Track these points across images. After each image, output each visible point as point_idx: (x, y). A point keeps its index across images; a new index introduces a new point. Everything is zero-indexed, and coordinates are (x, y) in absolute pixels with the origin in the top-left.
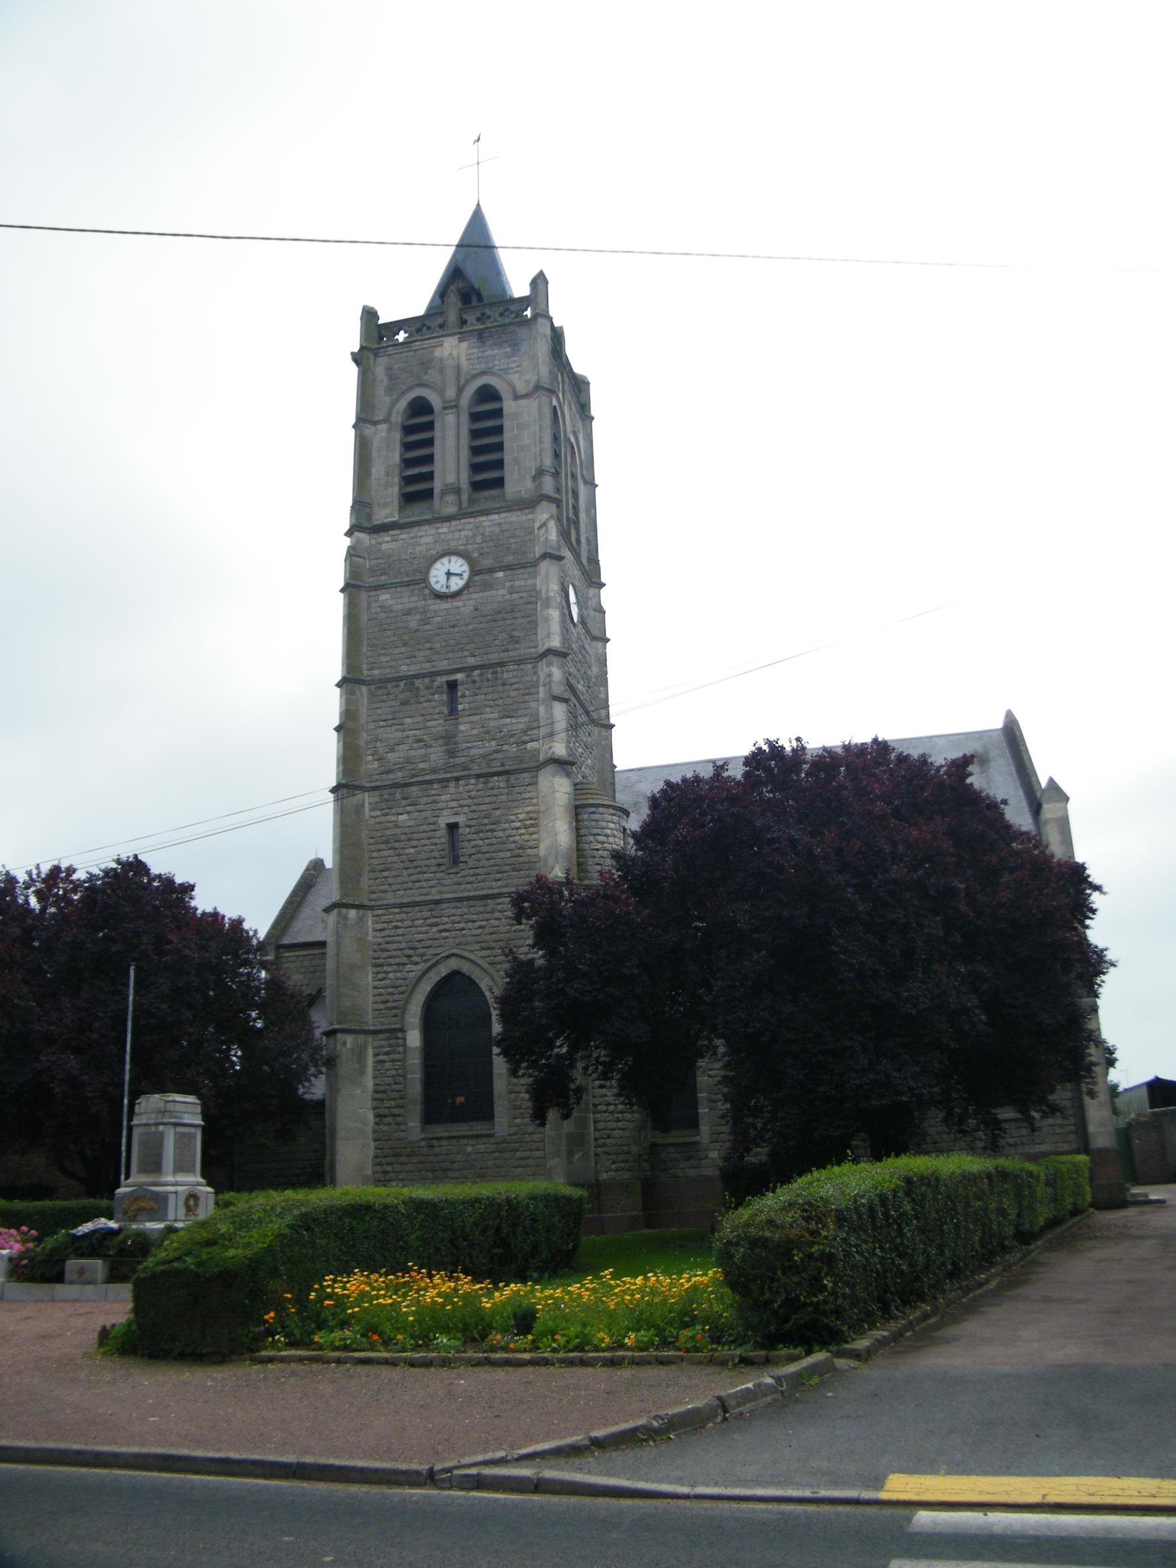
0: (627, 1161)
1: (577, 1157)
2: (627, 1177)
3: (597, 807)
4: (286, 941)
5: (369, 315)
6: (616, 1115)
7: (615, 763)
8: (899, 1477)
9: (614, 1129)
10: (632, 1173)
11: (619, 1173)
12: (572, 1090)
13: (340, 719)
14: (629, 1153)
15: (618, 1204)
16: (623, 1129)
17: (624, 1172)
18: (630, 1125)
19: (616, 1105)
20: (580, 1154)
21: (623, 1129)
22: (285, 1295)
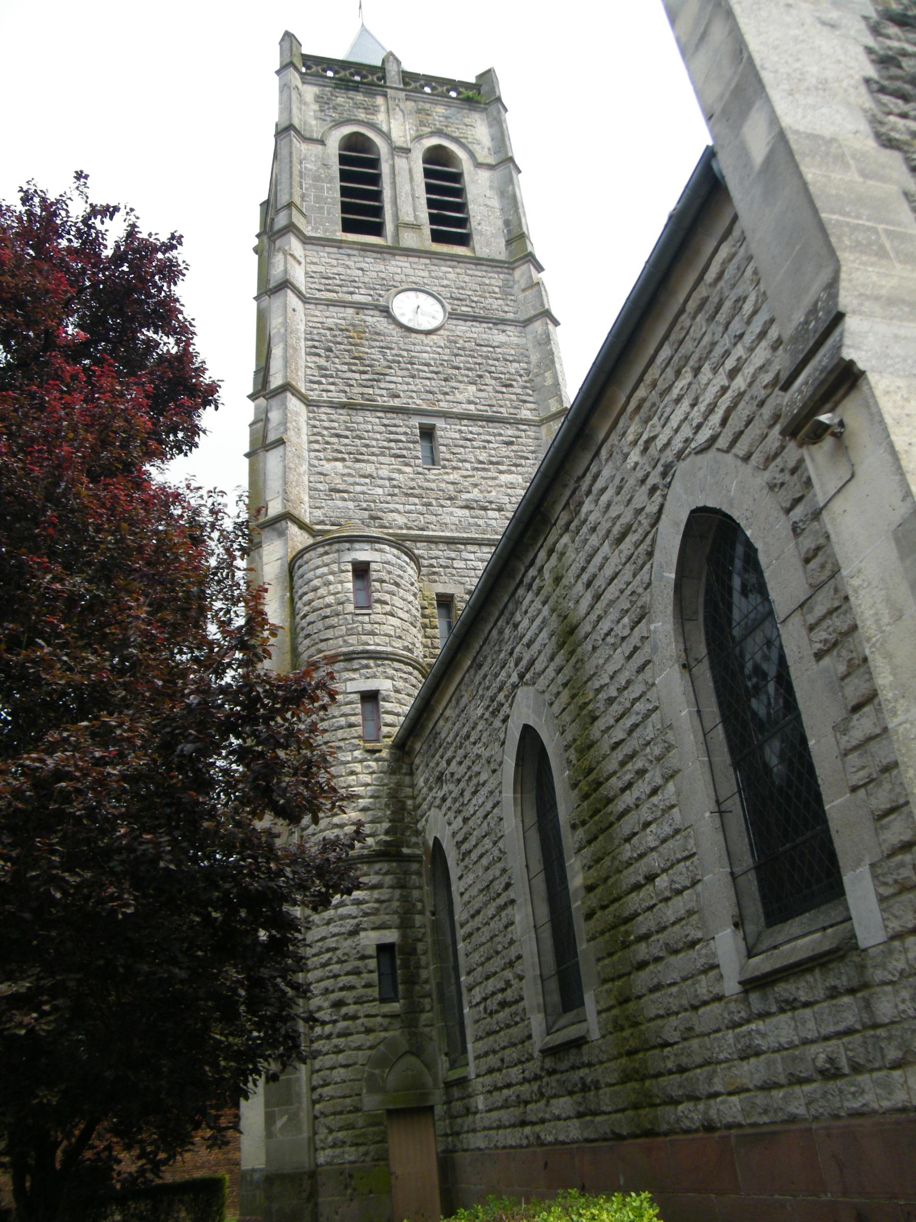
0: (350, 1127)
1: (279, 1124)
2: (352, 1158)
3: (302, 557)
4: (272, 284)
5: (289, 38)
6: (335, 1041)
7: (256, 257)
8: (403, 314)
9: (332, 1068)
10: (362, 1149)
11: (338, 1151)
12: (274, 704)
13: (255, 384)
14: (357, 1110)
15: (337, 1213)
16: (346, 1066)
17: (347, 1149)
18: (361, 1056)
19: (335, 1022)
20: (285, 1118)
21: (346, 1066)
22: (58, 1166)
